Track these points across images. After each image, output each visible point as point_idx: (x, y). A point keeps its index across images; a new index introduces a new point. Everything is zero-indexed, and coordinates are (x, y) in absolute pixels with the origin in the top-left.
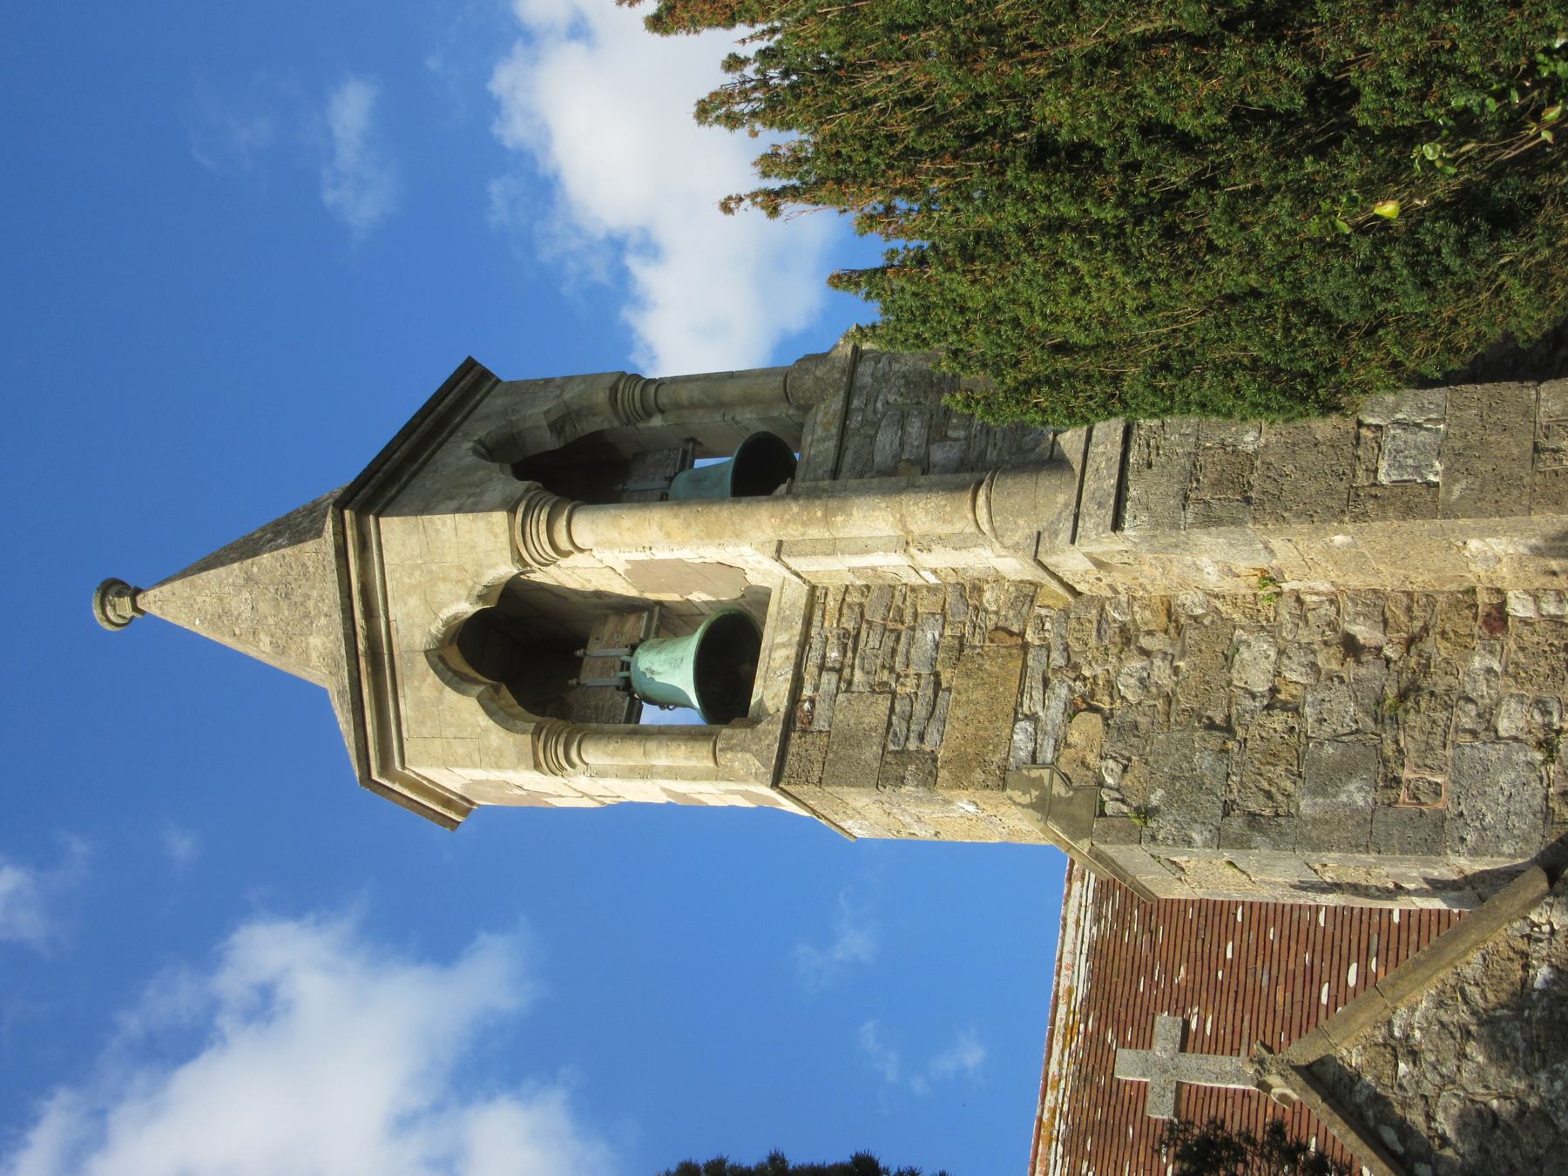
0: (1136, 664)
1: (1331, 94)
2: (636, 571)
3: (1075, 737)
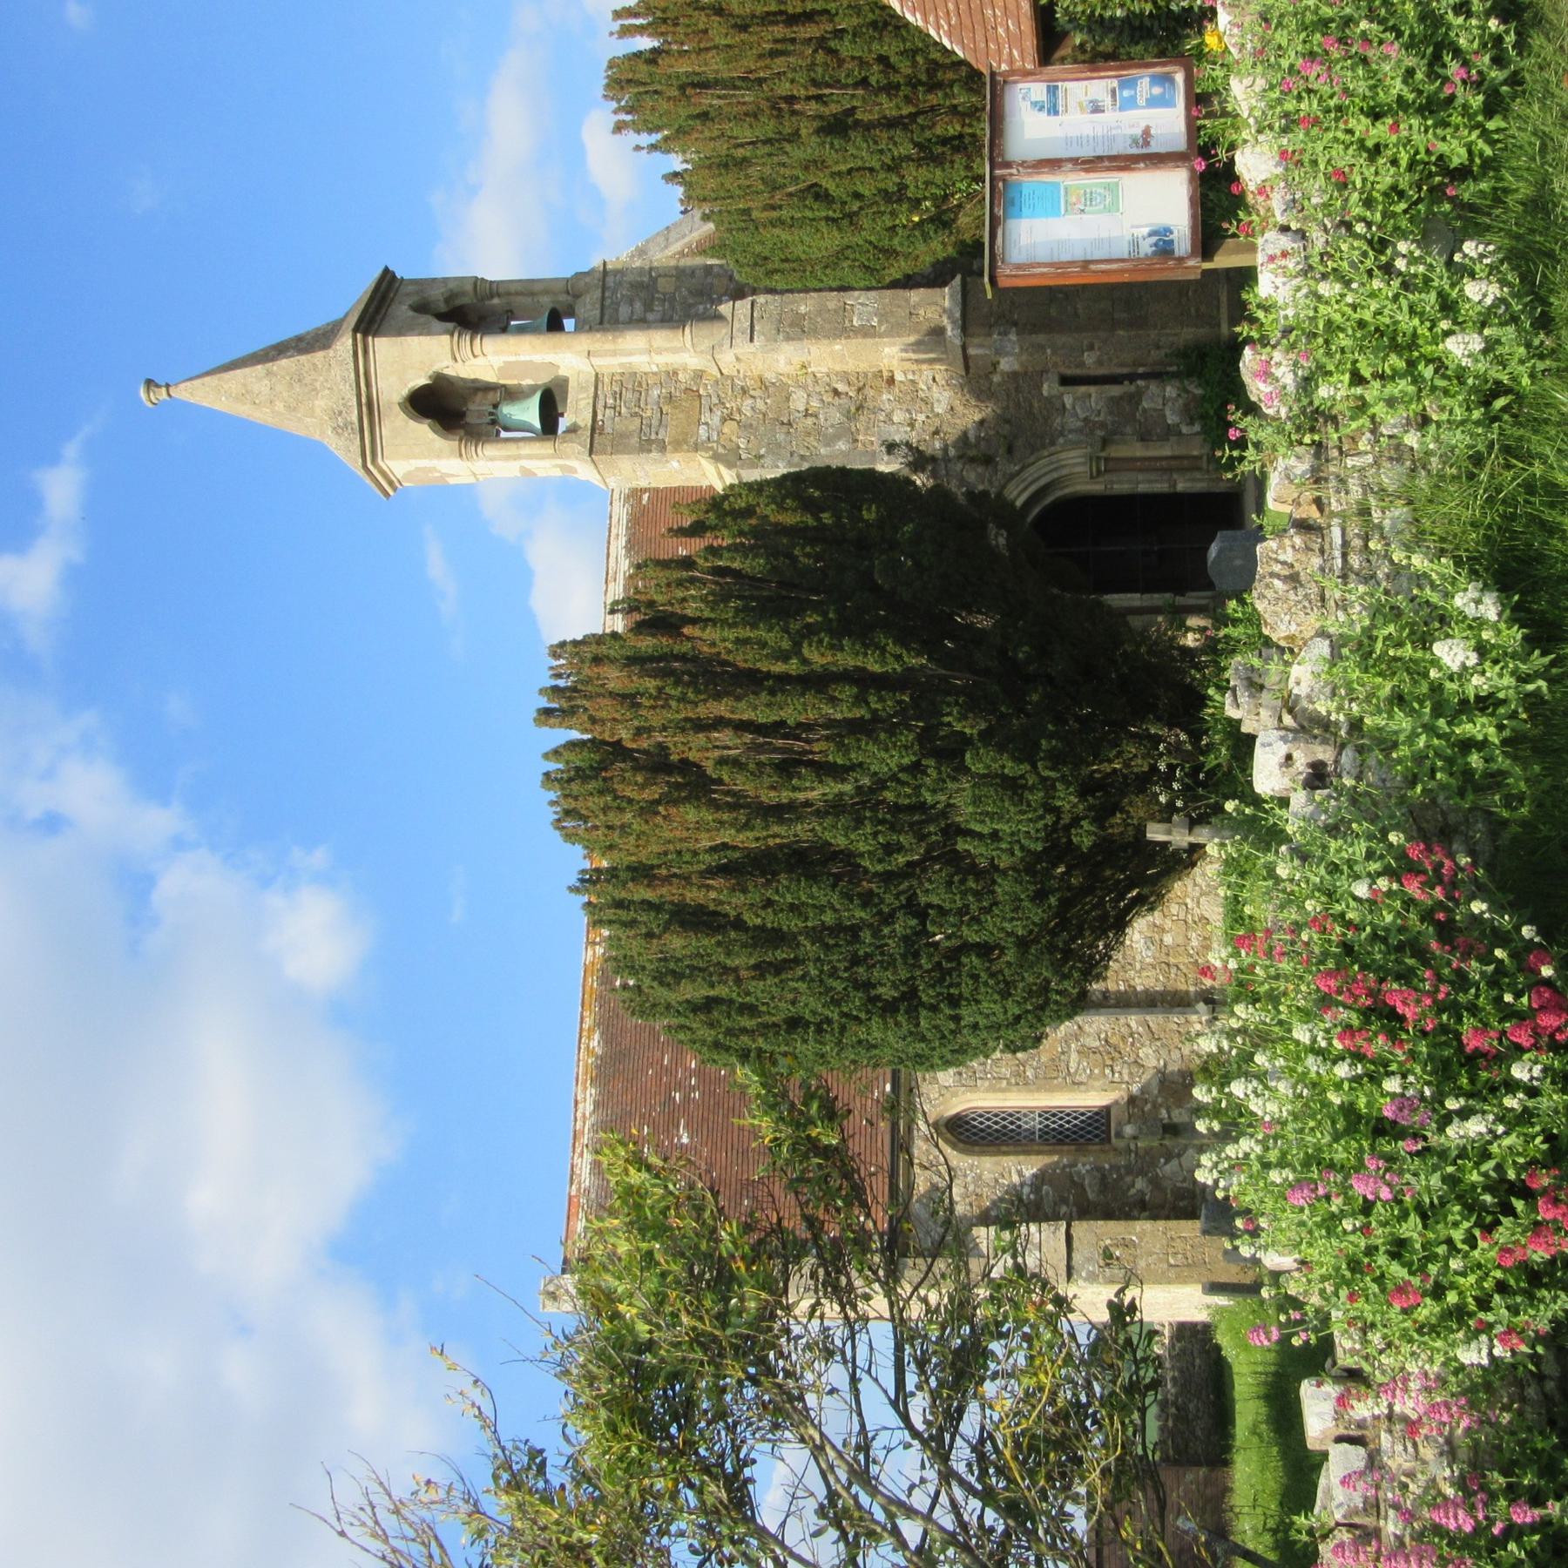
0: (750, 401)
1: (902, 187)
2: (506, 368)
3: (726, 430)
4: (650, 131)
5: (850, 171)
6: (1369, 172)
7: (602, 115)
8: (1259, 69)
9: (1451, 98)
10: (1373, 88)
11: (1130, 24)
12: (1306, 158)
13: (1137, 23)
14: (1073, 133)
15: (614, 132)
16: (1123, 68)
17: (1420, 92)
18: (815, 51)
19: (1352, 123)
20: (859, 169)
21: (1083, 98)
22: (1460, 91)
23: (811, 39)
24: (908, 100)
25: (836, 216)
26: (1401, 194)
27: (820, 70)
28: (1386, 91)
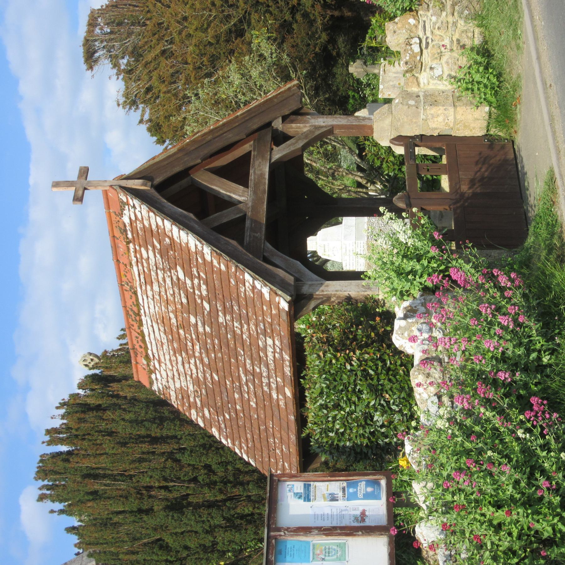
1: (215, 544)
4: (61, 501)
5: (182, 533)
6: (495, 539)
7: (33, 489)
8: (430, 476)
9: (541, 498)
10: (496, 490)
11: (355, 450)
12: (457, 529)
13: (359, 450)
14: (319, 512)
15: (38, 501)
16: (350, 476)
17: (523, 494)
18: (166, 460)
19: (485, 510)
20: (189, 531)
21: (325, 492)
22: (546, 494)
23: (164, 453)
24: (221, 491)
25: (172, 559)
26: (514, 553)
27: (168, 471)
28: (504, 491)
